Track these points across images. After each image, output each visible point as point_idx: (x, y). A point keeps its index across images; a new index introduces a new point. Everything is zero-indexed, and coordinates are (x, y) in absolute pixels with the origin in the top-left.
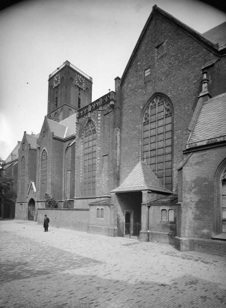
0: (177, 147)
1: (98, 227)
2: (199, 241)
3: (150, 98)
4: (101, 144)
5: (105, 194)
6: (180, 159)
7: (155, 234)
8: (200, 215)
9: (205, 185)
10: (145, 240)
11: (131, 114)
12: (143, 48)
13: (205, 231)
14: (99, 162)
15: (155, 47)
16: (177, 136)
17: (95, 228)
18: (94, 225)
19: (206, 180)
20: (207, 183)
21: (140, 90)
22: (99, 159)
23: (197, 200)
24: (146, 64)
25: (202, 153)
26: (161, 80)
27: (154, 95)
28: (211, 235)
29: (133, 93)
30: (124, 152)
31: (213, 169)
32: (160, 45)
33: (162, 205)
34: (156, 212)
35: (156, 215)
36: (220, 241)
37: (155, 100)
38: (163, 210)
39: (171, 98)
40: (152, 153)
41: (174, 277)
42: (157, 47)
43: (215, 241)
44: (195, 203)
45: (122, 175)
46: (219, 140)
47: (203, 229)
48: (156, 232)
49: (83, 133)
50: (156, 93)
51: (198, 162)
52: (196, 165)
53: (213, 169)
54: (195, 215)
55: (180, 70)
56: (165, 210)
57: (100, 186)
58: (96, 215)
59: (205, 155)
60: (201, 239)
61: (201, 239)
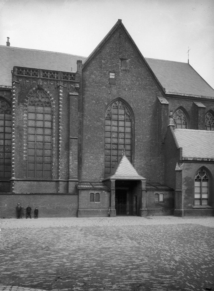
0: (137, 147)
1: (94, 211)
2: (187, 210)
3: (114, 100)
4: (63, 124)
5: (74, 178)
6: (139, 157)
7: (151, 210)
8: (188, 197)
9: (190, 181)
10: (146, 215)
11: (95, 105)
12: (107, 50)
13: (190, 205)
14: (62, 142)
15: (120, 58)
16: (137, 140)
17: (88, 211)
18: (87, 209)
19: (190, 178)
20: (191, 180)
21: (104, 87)
22: (62, 139)
23: (186, 188)
24: (110, 66)
25: (189, 164)
26: (125, 89)
27: (118, 98)
28: (192, 207)
29: (97, 86)
30: (87, 139)
31: (194, 173)
32: (125, 59)
33: (155, 191)
34: (151, 195)
35: (151, 197)
36: (196, 209)
37: (117, 102)
38: (156, 194)
39: (133, 109)
40: (114, 147)
41: (91, 250)
42: (122, 59)
43: (194, 209)
44: (185, 190)
45: (84, 160)
46: (198, 160)
47: (189, 204)
48: (152, 209)
49: (27, 99)
50: (120, 98)
51: (187, 168)
52: (186, 170)
53: (194, 173)
54: (185, 197)
55: (140, 91)
56: (158, 194)
57: (63, 168)
58: (89, 199)
59: (190, 165)
60: (188, 209)
61: (188, 209)
